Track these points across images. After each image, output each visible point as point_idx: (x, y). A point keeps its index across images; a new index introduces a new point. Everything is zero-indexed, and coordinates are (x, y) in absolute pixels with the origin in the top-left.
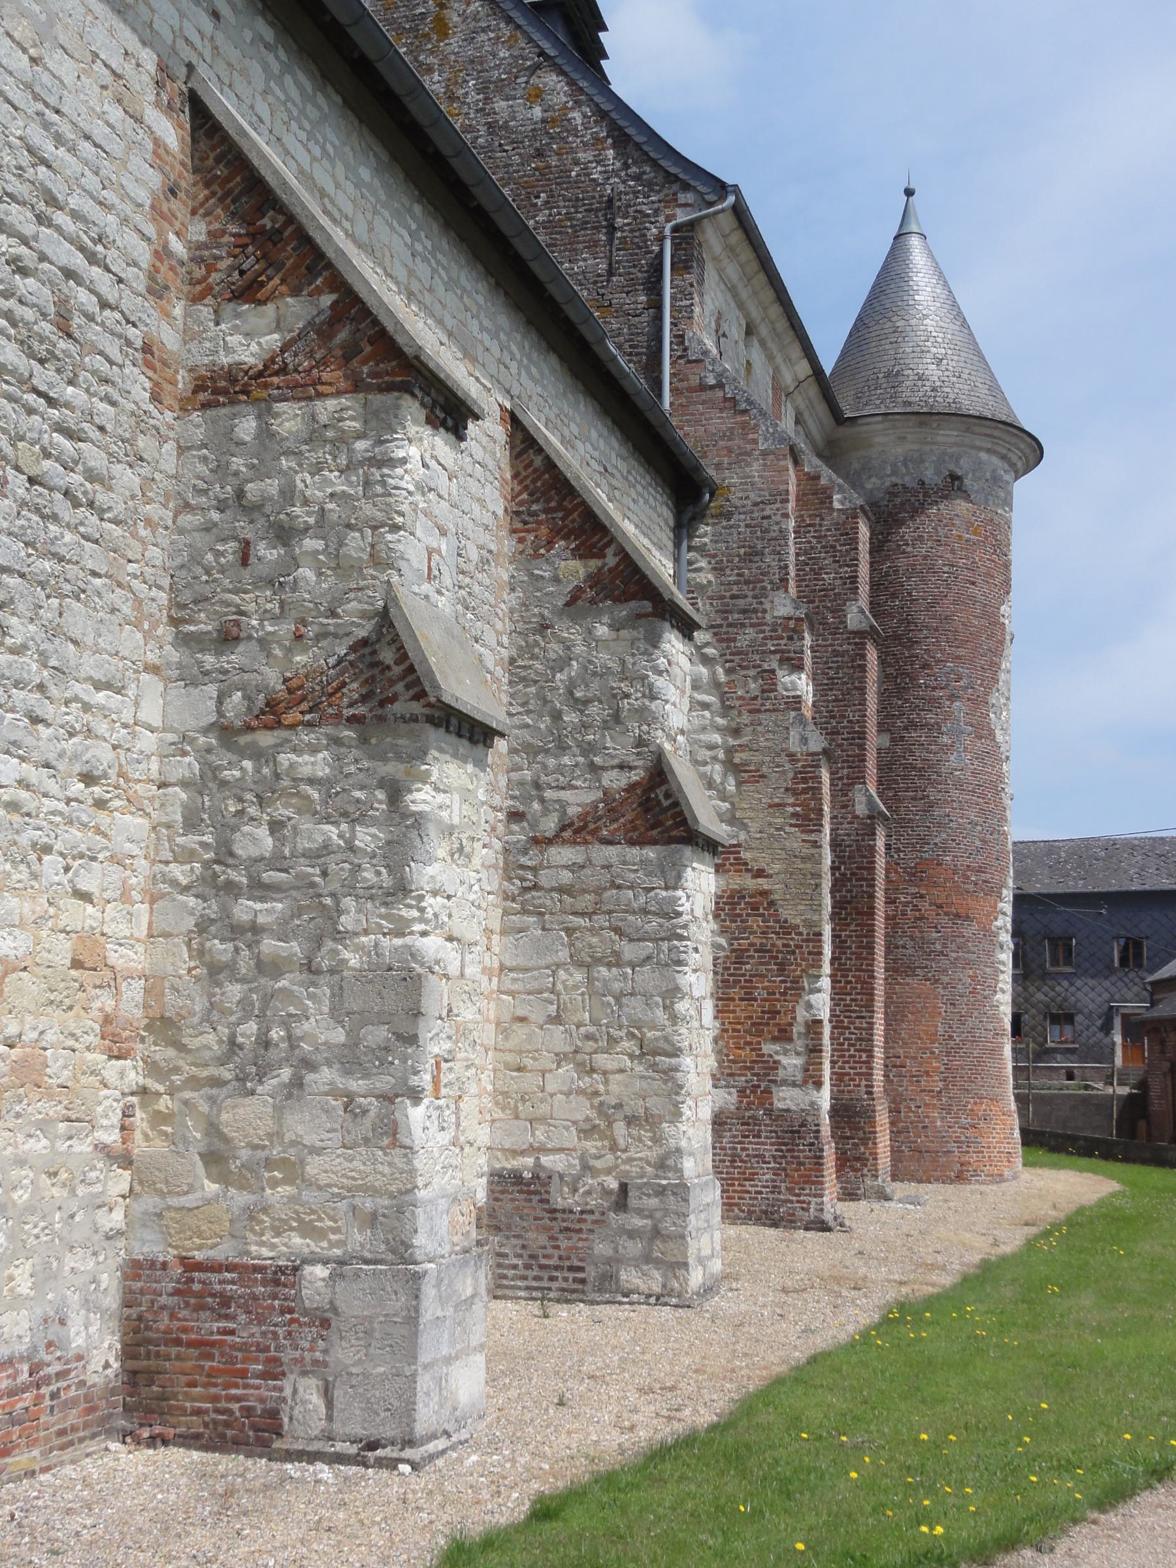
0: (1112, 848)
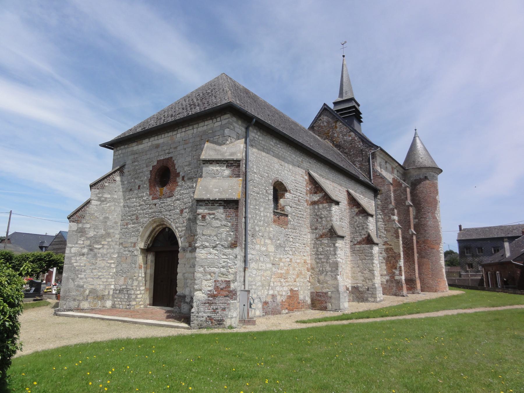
0: (483, 230)
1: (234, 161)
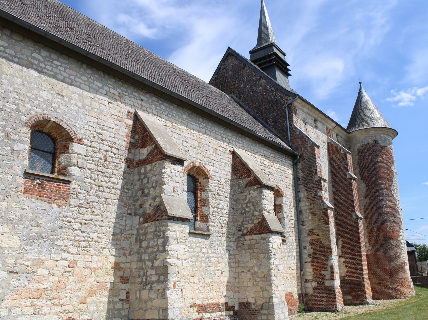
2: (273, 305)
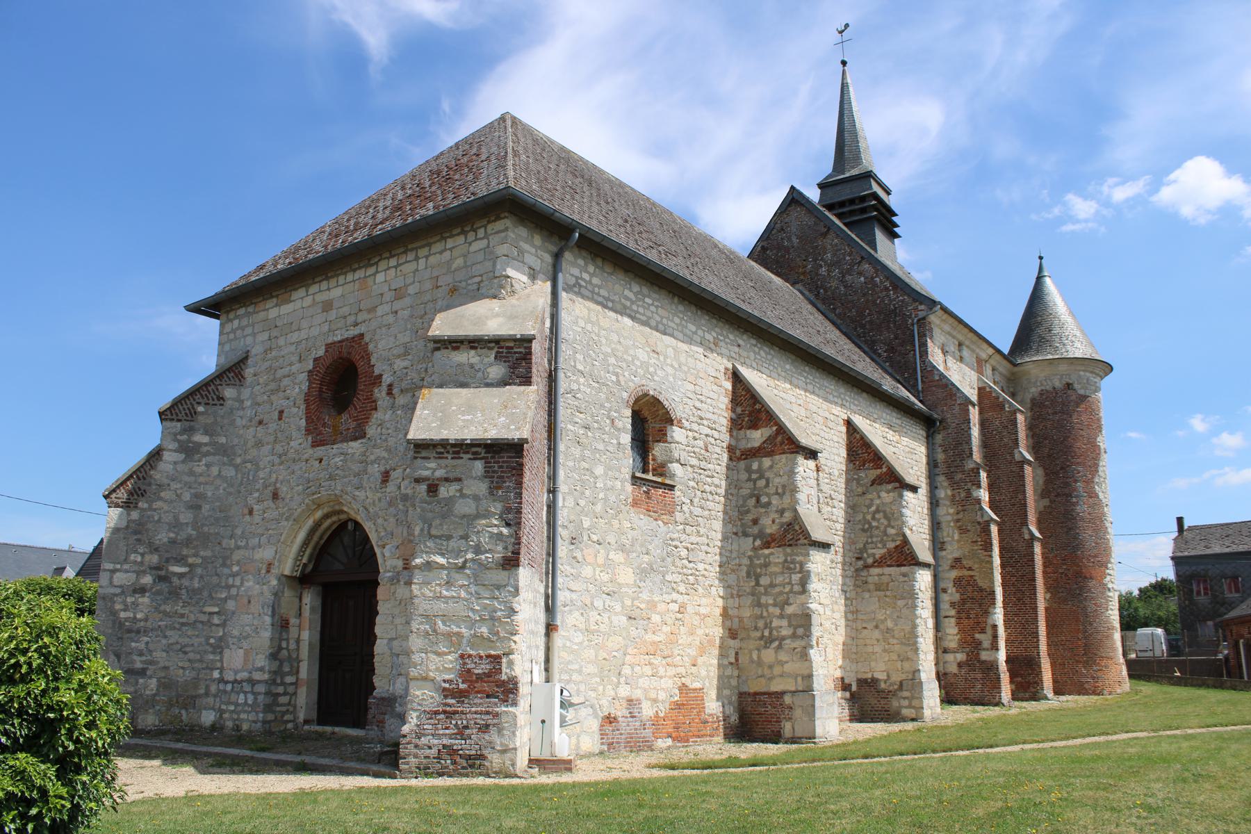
1: (515, 340)
2: (921, 683)
